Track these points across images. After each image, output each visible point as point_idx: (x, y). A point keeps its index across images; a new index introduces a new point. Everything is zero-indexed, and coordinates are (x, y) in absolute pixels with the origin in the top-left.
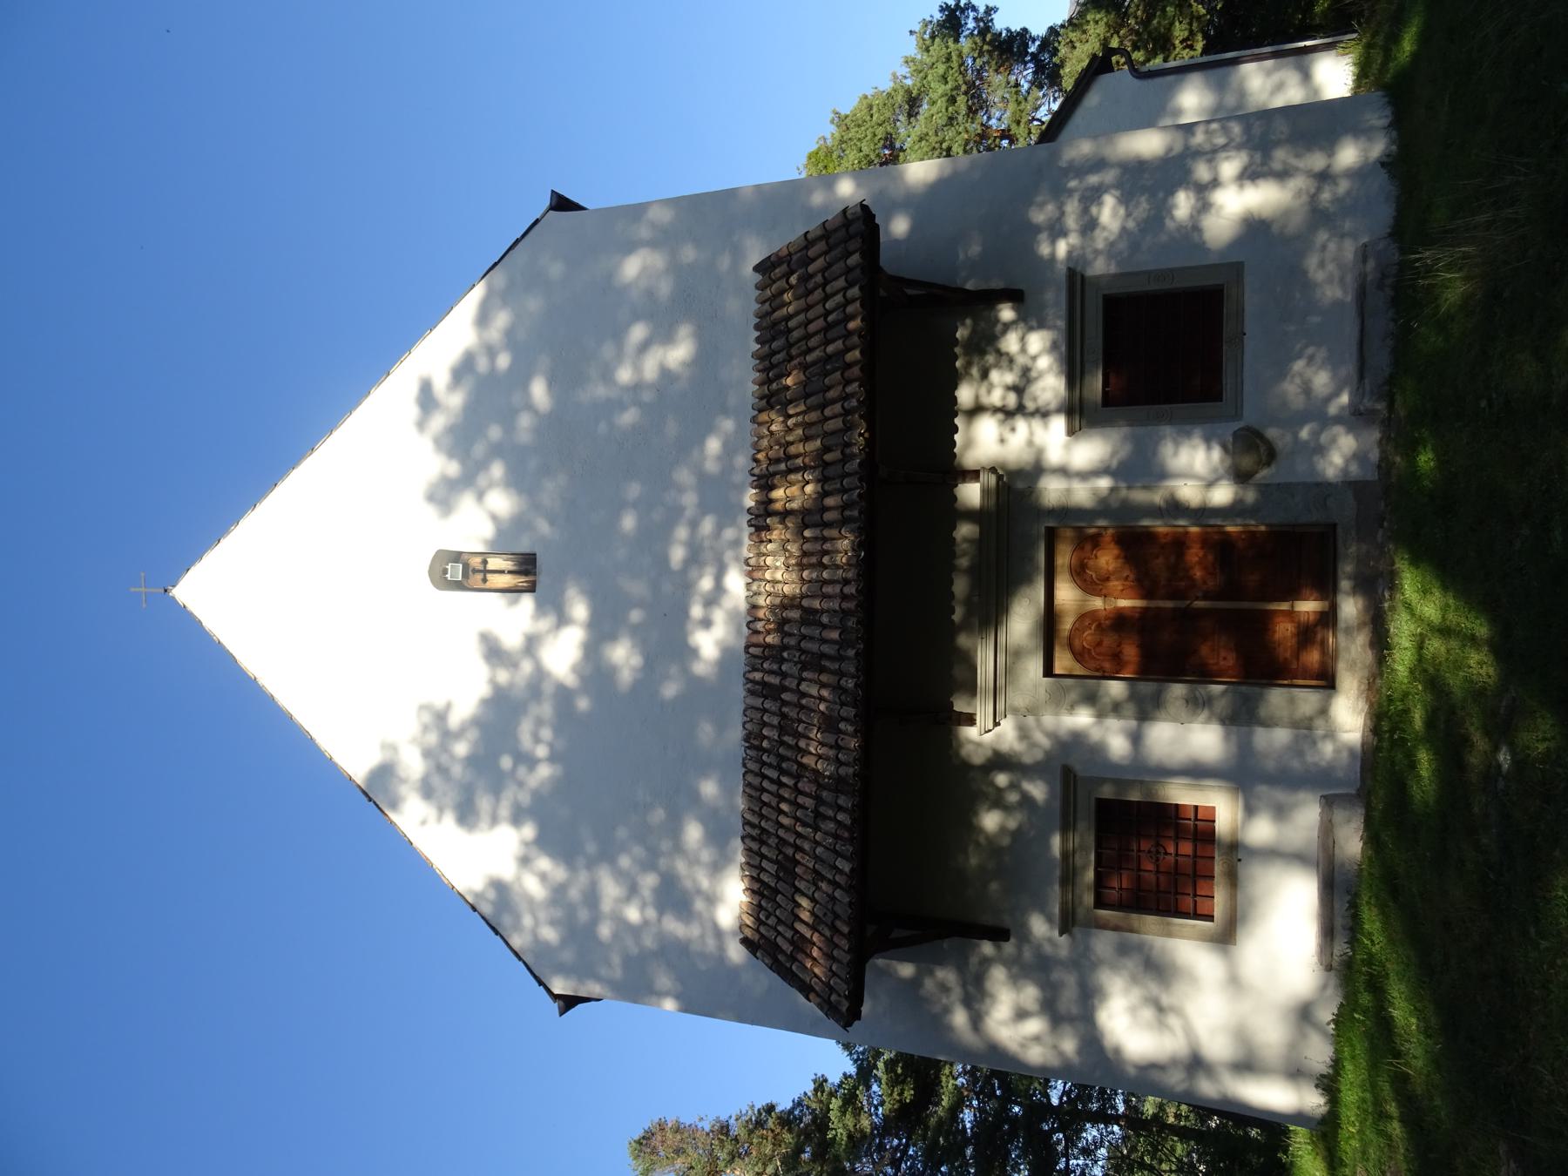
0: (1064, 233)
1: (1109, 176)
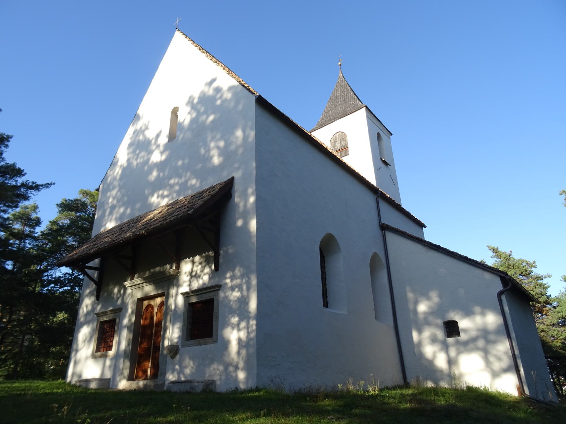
0: (232, 281)
1: (245, 293)
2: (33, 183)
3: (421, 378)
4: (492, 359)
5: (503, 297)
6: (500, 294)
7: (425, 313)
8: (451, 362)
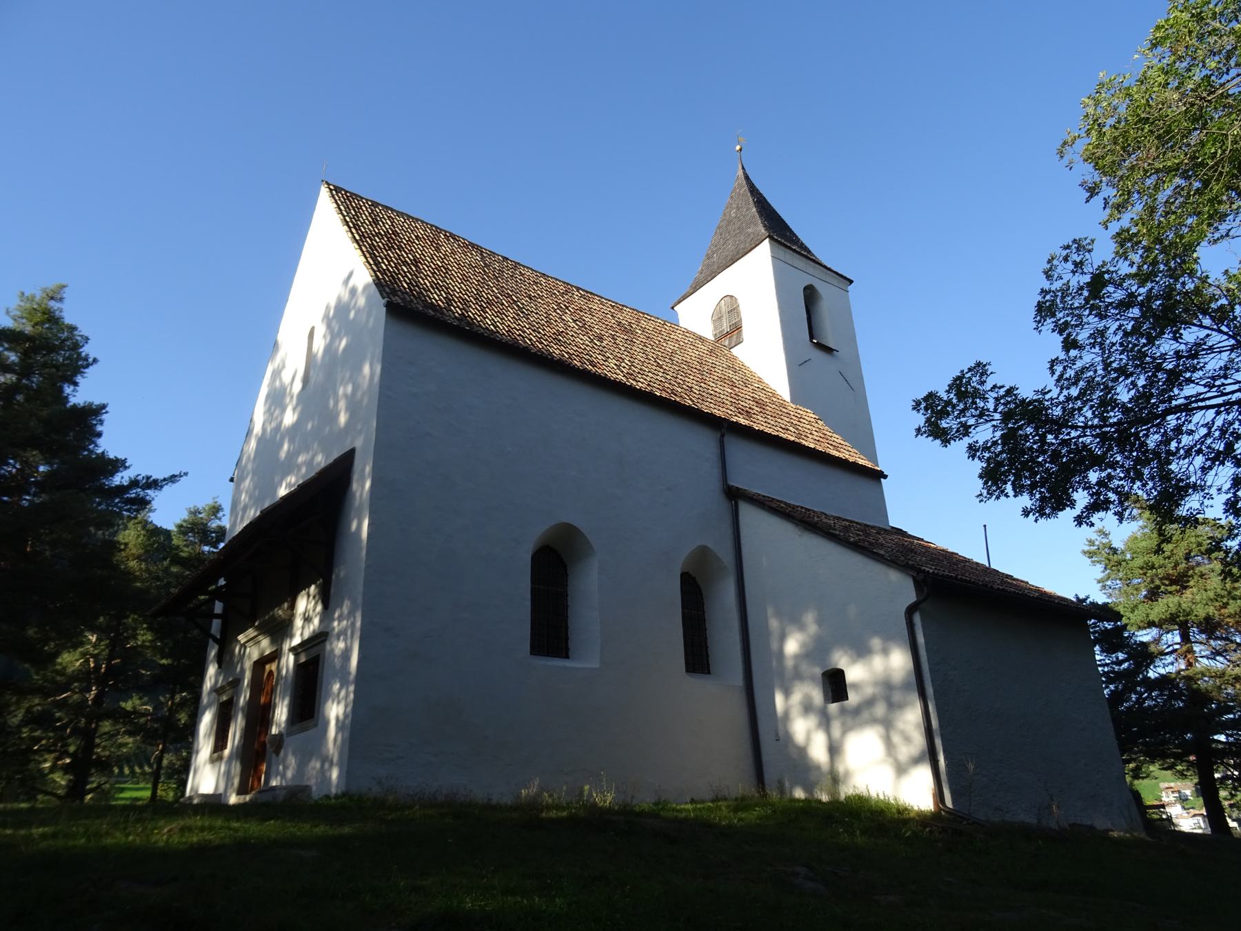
0: (339, 622)
2: (148, 478)
3: (787, 784)
4: (896, 739)
5: (917, 618)
6: (910, 611)
7: (796, 657)
8: (834, 750)
